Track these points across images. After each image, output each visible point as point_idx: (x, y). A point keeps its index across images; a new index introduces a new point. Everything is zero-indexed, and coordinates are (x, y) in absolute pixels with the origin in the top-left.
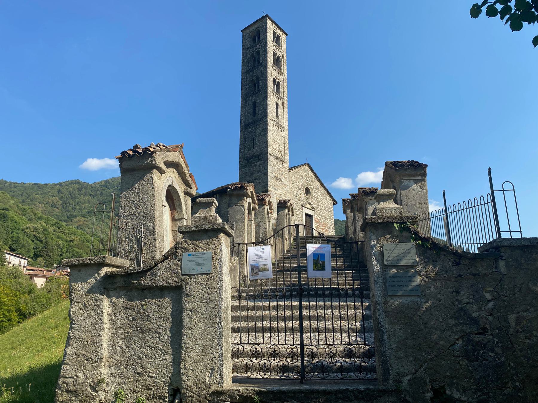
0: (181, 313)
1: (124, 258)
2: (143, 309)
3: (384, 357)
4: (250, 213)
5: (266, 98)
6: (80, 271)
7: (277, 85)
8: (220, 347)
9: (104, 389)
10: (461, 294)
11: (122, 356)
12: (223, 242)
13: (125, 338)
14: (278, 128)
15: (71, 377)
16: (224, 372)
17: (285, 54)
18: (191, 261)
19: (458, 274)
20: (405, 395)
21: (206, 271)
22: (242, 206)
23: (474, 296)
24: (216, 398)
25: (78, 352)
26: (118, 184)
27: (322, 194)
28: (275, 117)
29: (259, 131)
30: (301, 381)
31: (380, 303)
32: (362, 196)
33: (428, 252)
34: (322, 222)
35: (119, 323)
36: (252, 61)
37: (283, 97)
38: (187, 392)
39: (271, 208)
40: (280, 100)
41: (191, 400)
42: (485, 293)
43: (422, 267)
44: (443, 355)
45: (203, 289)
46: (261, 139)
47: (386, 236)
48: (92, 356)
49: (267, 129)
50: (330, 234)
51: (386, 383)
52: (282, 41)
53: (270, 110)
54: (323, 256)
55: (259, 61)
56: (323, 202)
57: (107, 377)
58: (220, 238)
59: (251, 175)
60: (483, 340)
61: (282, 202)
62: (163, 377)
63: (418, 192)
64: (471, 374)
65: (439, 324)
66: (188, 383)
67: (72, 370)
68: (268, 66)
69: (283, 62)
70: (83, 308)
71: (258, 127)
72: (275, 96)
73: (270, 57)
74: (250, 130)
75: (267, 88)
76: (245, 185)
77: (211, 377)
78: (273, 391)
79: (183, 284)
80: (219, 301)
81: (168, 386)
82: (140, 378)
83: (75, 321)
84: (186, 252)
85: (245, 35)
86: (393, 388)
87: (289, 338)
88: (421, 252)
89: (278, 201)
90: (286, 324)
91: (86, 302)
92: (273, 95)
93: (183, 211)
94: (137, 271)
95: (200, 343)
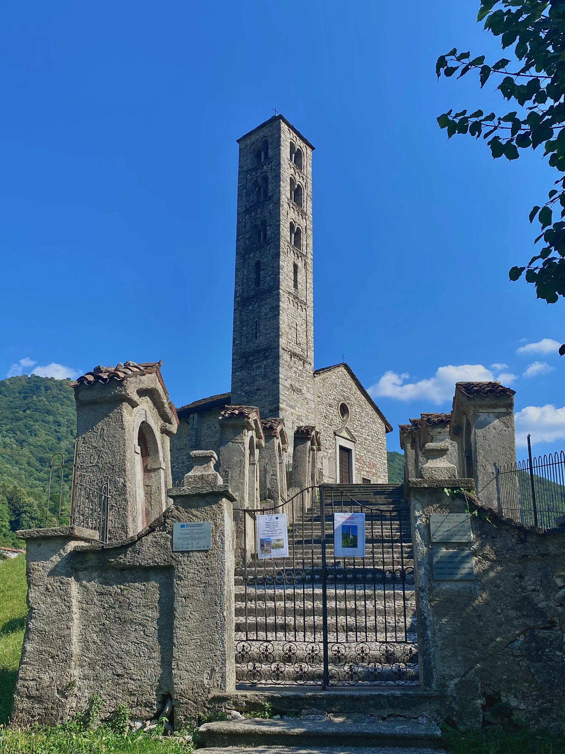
0: (172, 599)
1: (83, 526)
2: (123, 595)
3: (427, 657)
4: (252, 454)
5: (278, 255)
6: (39, 545)
7: (296, 233)
8: (222, 643)
9: (76, 695)
10: (526, 580)
11: (96, 654)
12: (225, 509)
13: (100, 631)
14: (296, 306)
15: (33, 680)
16: (227, 674)
17: (310, 182)
18: (185, 534)
19: (523, 554)
20: (451, 703)
21: (204, 547)
22: (240, 443)
23: (541, 582)
24: (217, 705)
25: (41, 648)
26: (21, 388)
27: (367, 414)
28: (292, 288)
29: (265, 310)
30: (324, 689)
31: (424, 589)
32: (427, 427)
33: (486, 525)
34: (368, 461)
35: (91, 613)
36: (255, 193)
37: (305, 254)
38: (180, 698)
39: (284, 442)
40: (300, 258)
41: (186, 707)
42: (555, 578)
43: (477, 544)
44: (500, 654)
45: (200, 570)
46: (268, 323)
47: (434, 505)
48: (59, 653)
49: (279, 306)
50: (380, 482)
51: (429, 688)
52: (306, 160)
53: (285, 275)
54: (355, 528)
55: (266, 193)
56: (369, 428)
57: (79, 680)
58: (222, 504)
59: (250, 383)
60: (550, 636)
61: (302, 431)
62: (149, 679)
63: (500, 432)
64: (533, 677)
65: (496, 616)
66: (181, 686)
67: (34, 670)
68: (281, 203)
69: (305, 194)
70: (45, 593)
71: (263, 303)
72: (292, 252)
73: (285, 186)
74: (250, 308)
75: (279, 239)
76: (246, 411)
77: (210, 679)
78: (288, 697)
79: (174, 563)
80: (221, 585)
81: (156, 691)
82: (121, 681)
83: (35, 609)
84: (178, 522)
85: (244, 149)
86: (436, 694)
87: (309, 638)
88: (477, 526)
89: (296, 429)
90: (306, 620)
91: (49, 587)
92: (289, 250)
93: (160, 458)
94: (115, 546)
95: (196, 638)
